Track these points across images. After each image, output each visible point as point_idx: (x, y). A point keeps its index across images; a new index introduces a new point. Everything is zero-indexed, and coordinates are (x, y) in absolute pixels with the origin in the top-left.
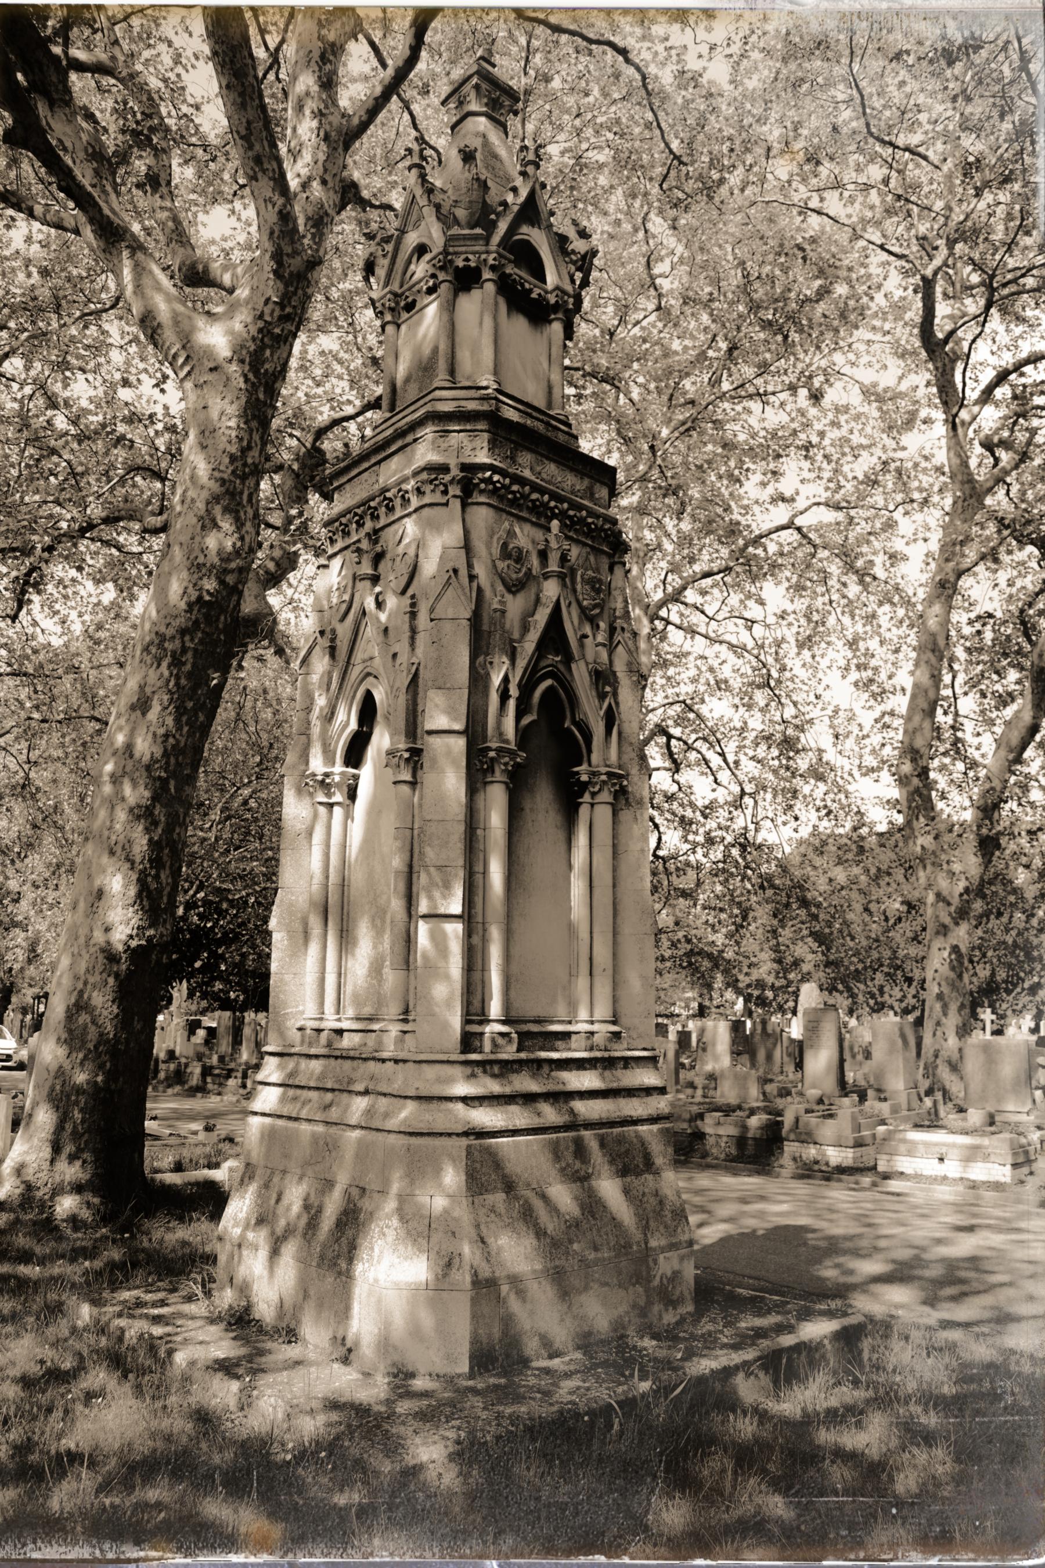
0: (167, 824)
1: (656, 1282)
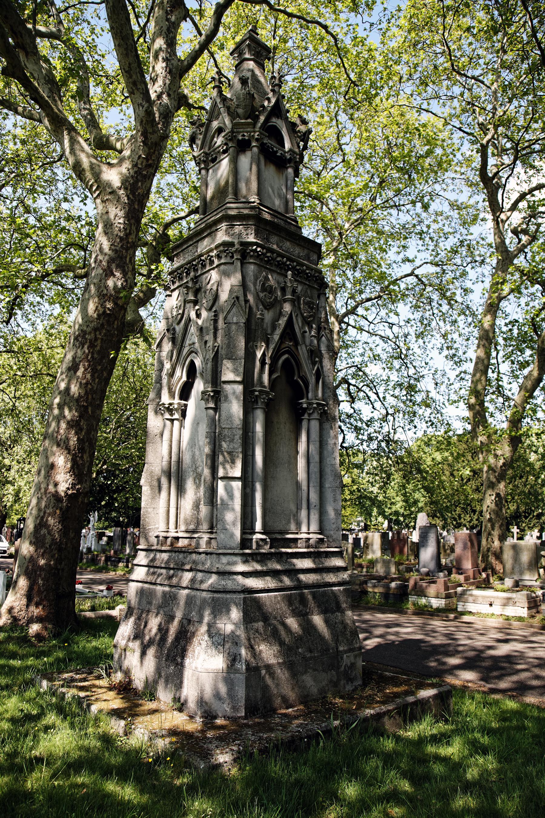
0: (87, 430)
1: (342, 669)
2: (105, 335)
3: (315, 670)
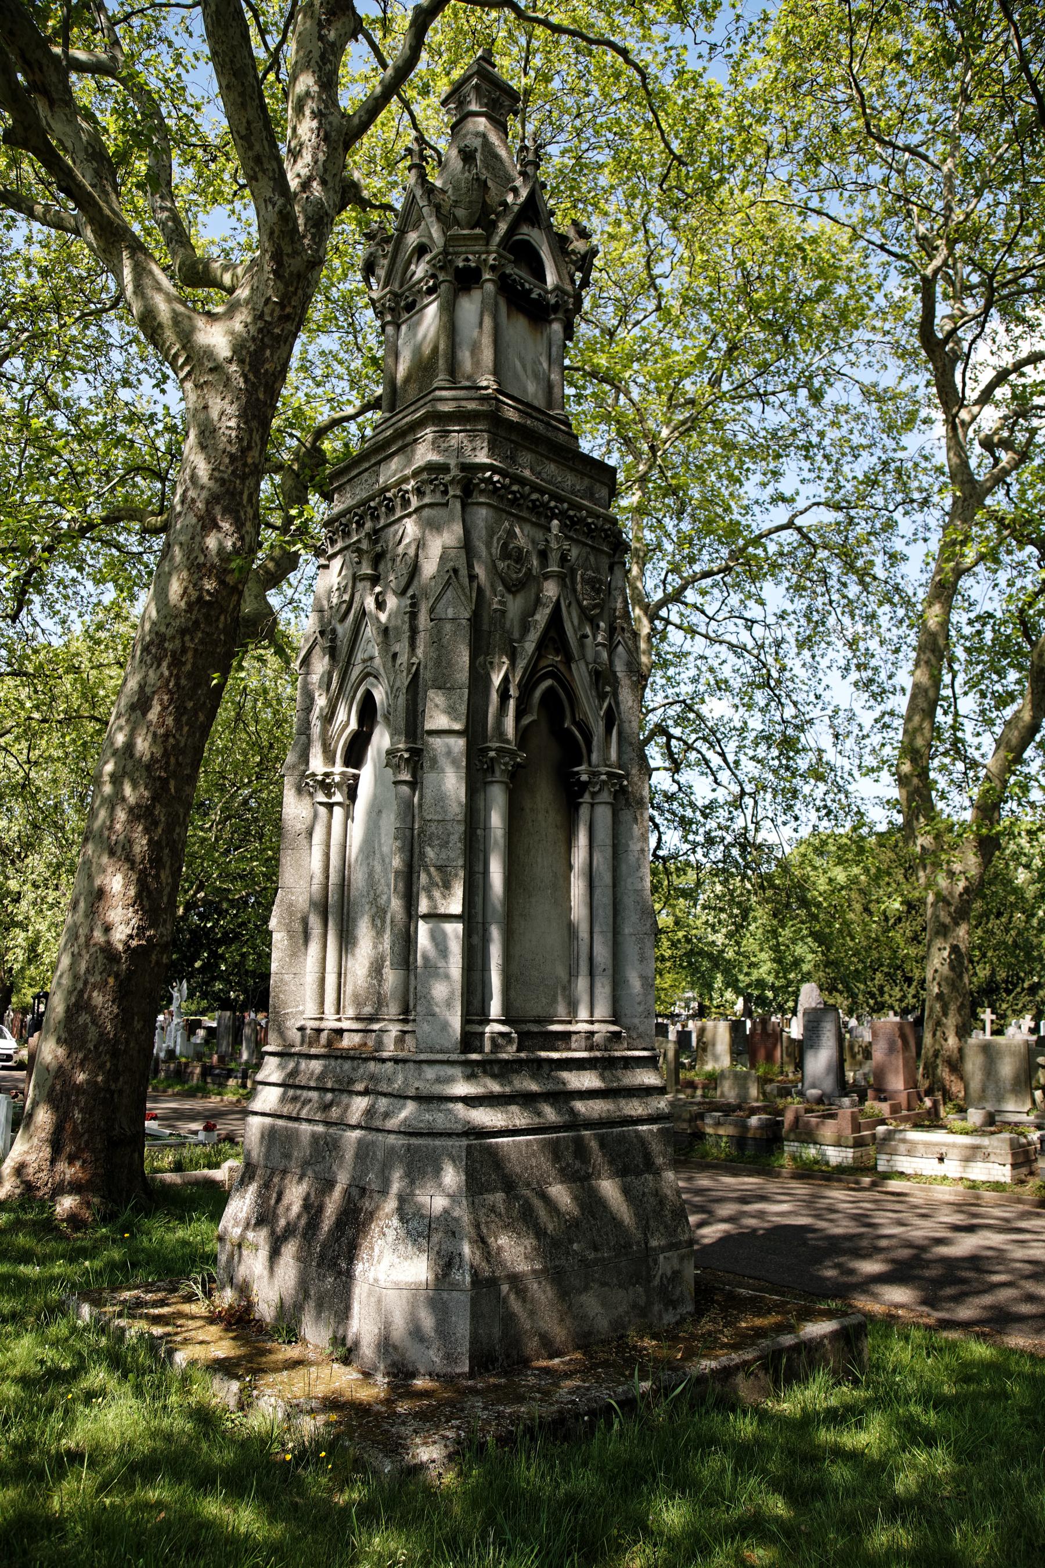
1: (656, 1282)
2: (202, 642)
3: (604, 1284)
